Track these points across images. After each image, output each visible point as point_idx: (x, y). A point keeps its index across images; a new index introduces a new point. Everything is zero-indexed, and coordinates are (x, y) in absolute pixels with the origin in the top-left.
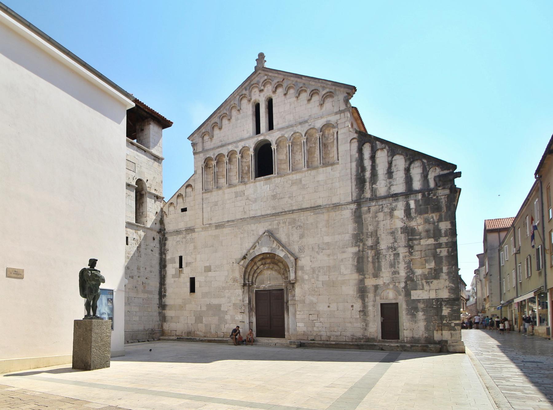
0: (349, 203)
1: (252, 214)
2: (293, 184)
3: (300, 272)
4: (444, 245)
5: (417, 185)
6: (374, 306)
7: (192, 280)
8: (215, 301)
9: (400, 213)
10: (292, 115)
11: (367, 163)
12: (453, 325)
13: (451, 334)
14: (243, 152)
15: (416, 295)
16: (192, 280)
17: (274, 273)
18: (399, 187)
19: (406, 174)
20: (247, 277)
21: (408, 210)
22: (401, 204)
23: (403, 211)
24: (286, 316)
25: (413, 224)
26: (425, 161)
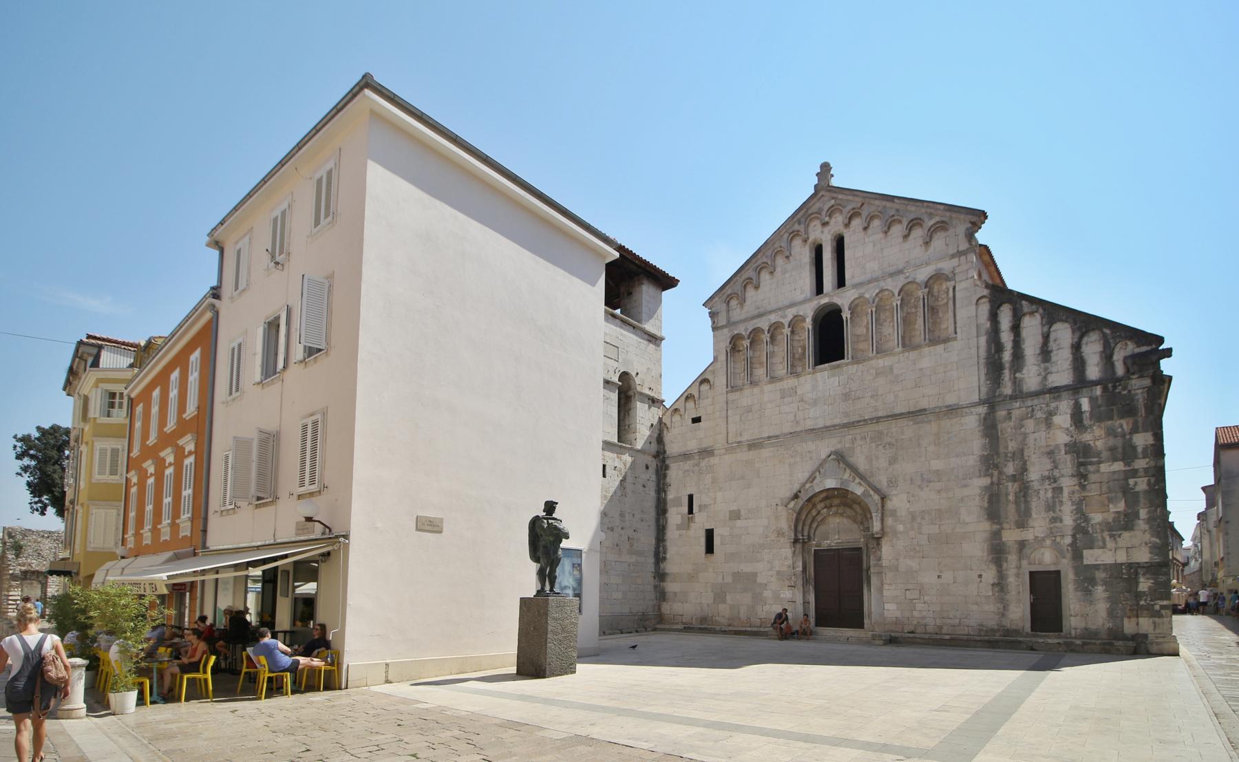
1: (810, 424)
5: (1093, 371)
7: (710, 534)
9: (1063, 419)
11: (1006, 338)
12: (1157, 607)
13: (1154, 623)
16: (710, 534)
17: (845, 521)
18: (1062, 375)
20: (800, 528)
26: (1107, 331)
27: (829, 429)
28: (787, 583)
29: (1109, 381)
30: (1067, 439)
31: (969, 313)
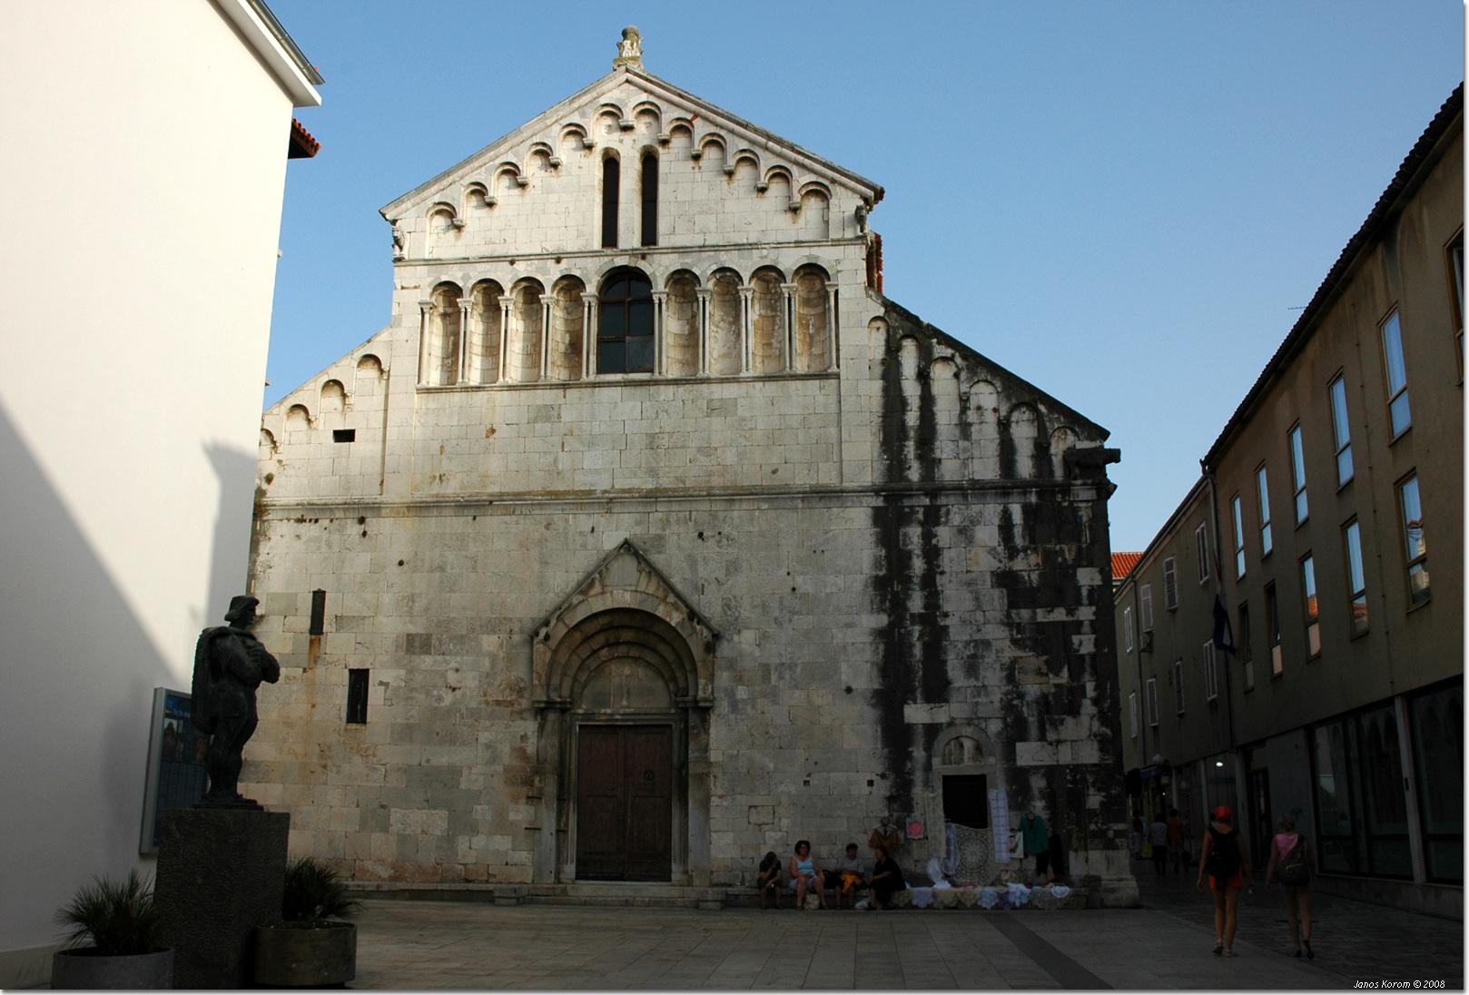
0: (863, 491)
1: (581, 482)
2: (711, 410)
3: (725, 674)
4: (1086, 628)
5: (1025, 467)
6: (927, 784)
7: (359, 680)
8: (443, 757)
9: (988, 534)
10: (713, 218)
11: (911, 389)
12: (1111, 834)
13: (1107, 858)
14: (571, 284)
15: (1029, 753)
16: (359, 680)
17: (641, 672)
18: (987, 469)
19: (1000, 433)
21: (1006, 527)
22: (992, 511)
23: (996, 530)
24: (675, 811)
25: (1019, 564)
26: (1042, 408)
27: (610, 502)
28: (524, 790)
29: (1042, 482)
30: (995, 565)
31: (861, 341)
